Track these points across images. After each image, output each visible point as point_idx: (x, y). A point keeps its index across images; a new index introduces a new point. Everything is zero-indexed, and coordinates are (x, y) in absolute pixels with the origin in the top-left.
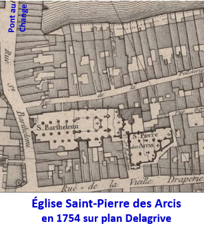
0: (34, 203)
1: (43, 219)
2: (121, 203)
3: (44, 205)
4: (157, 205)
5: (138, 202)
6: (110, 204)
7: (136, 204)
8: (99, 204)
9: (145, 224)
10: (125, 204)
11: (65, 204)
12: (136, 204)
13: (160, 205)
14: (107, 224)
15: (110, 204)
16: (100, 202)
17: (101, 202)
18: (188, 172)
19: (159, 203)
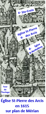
0: (1, 101)
1: (16, 106)
2: (24, 100)
3: (5, 101)
4: (36, 101)
5: (22, 110)
6: (32, 30)
7: (29, 101)
8: (17, 101)
9: (31, 26)
10: (25, 101)
11: (25, 32)
12: (29, 101)
13: (37, 101)
14: (14, 113)
15: (32, 30)
16: (30, 30)
17: (18, 100)
18: (20, 78)
19: (31, 34)
